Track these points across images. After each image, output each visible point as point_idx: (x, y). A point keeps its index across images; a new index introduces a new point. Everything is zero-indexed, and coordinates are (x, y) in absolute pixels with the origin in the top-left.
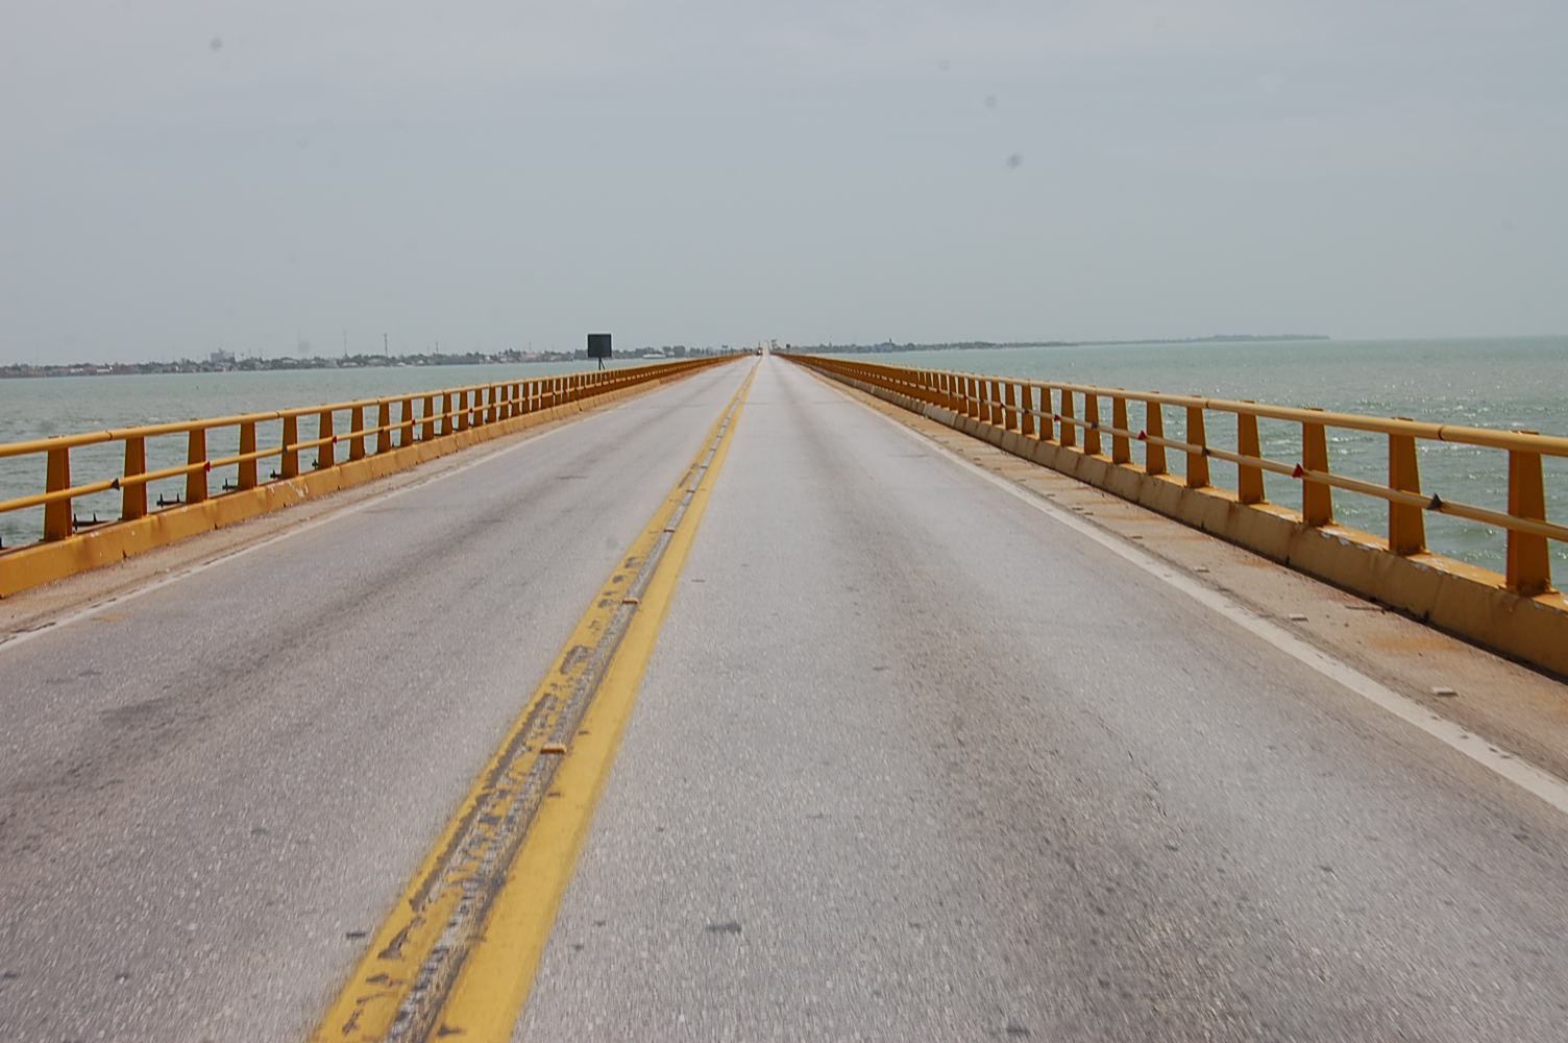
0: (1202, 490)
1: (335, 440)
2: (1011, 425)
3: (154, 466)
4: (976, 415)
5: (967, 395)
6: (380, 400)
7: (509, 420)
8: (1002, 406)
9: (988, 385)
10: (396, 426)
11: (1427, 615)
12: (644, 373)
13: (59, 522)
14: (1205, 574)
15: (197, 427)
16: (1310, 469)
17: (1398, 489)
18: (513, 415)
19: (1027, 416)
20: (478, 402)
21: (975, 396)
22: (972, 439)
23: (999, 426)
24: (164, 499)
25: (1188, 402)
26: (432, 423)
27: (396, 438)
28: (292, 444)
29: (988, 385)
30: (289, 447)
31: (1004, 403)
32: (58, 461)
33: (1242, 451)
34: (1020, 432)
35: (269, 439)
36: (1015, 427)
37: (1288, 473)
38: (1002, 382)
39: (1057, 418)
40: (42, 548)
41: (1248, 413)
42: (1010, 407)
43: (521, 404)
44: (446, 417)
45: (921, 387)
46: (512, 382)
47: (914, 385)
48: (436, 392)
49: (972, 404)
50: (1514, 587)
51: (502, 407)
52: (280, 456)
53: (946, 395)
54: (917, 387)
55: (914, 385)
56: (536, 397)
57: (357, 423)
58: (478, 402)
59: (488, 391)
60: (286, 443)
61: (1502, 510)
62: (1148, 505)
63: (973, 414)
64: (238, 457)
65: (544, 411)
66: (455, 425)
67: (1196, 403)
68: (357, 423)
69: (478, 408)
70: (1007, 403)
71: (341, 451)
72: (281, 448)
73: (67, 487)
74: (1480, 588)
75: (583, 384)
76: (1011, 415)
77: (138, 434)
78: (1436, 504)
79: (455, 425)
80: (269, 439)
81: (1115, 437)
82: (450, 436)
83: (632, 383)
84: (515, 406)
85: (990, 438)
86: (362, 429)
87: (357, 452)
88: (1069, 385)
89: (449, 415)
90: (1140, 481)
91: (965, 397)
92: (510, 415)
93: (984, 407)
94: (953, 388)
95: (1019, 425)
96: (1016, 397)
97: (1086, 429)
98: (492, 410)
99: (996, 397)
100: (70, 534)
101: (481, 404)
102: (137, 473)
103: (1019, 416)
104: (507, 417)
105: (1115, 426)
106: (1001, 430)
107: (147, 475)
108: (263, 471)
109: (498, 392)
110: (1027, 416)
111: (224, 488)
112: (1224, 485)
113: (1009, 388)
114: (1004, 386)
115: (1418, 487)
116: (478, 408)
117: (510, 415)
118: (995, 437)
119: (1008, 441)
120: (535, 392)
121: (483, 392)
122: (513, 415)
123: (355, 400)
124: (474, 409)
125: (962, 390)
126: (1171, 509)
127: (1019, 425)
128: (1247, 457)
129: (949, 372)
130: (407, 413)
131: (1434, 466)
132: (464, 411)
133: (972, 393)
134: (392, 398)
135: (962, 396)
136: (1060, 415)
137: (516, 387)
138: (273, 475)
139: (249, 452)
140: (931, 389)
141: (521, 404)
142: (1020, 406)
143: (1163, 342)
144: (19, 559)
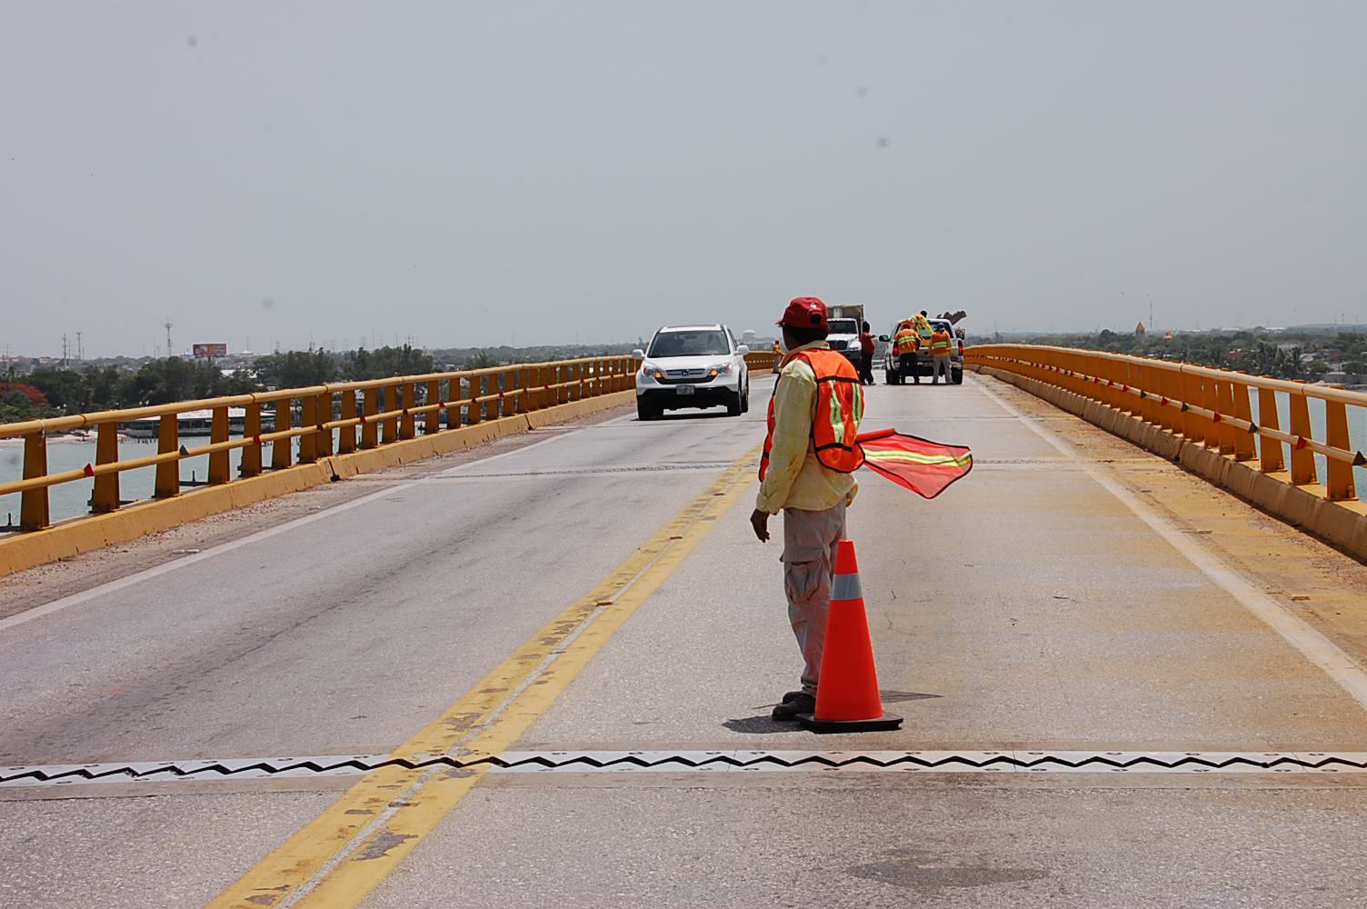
1: (184, 453)
7: (264, 475)
8: (1254, 429)
13: (35, 513)
19: (1301, 446)
22: (1349, 560)
24: (197, 480)
25: (1259, 383)
26: (226, 452)
31: (1257, 421)
42: (1269, 431)
47: (1179, 404)
54: (1143, 395)
70: (1262, 425)
73: (45, 474)
76: (1272, 446)
83: (525, 405)
86: (116, 461)
92: (380, 426)
102: (223, 441)
103: (1286, 450)
105: (1330, 444)
107: (120, 463)
110: (1301, 446)
115: (1349, 446)
122: (342, 451)
124: (95, 468)
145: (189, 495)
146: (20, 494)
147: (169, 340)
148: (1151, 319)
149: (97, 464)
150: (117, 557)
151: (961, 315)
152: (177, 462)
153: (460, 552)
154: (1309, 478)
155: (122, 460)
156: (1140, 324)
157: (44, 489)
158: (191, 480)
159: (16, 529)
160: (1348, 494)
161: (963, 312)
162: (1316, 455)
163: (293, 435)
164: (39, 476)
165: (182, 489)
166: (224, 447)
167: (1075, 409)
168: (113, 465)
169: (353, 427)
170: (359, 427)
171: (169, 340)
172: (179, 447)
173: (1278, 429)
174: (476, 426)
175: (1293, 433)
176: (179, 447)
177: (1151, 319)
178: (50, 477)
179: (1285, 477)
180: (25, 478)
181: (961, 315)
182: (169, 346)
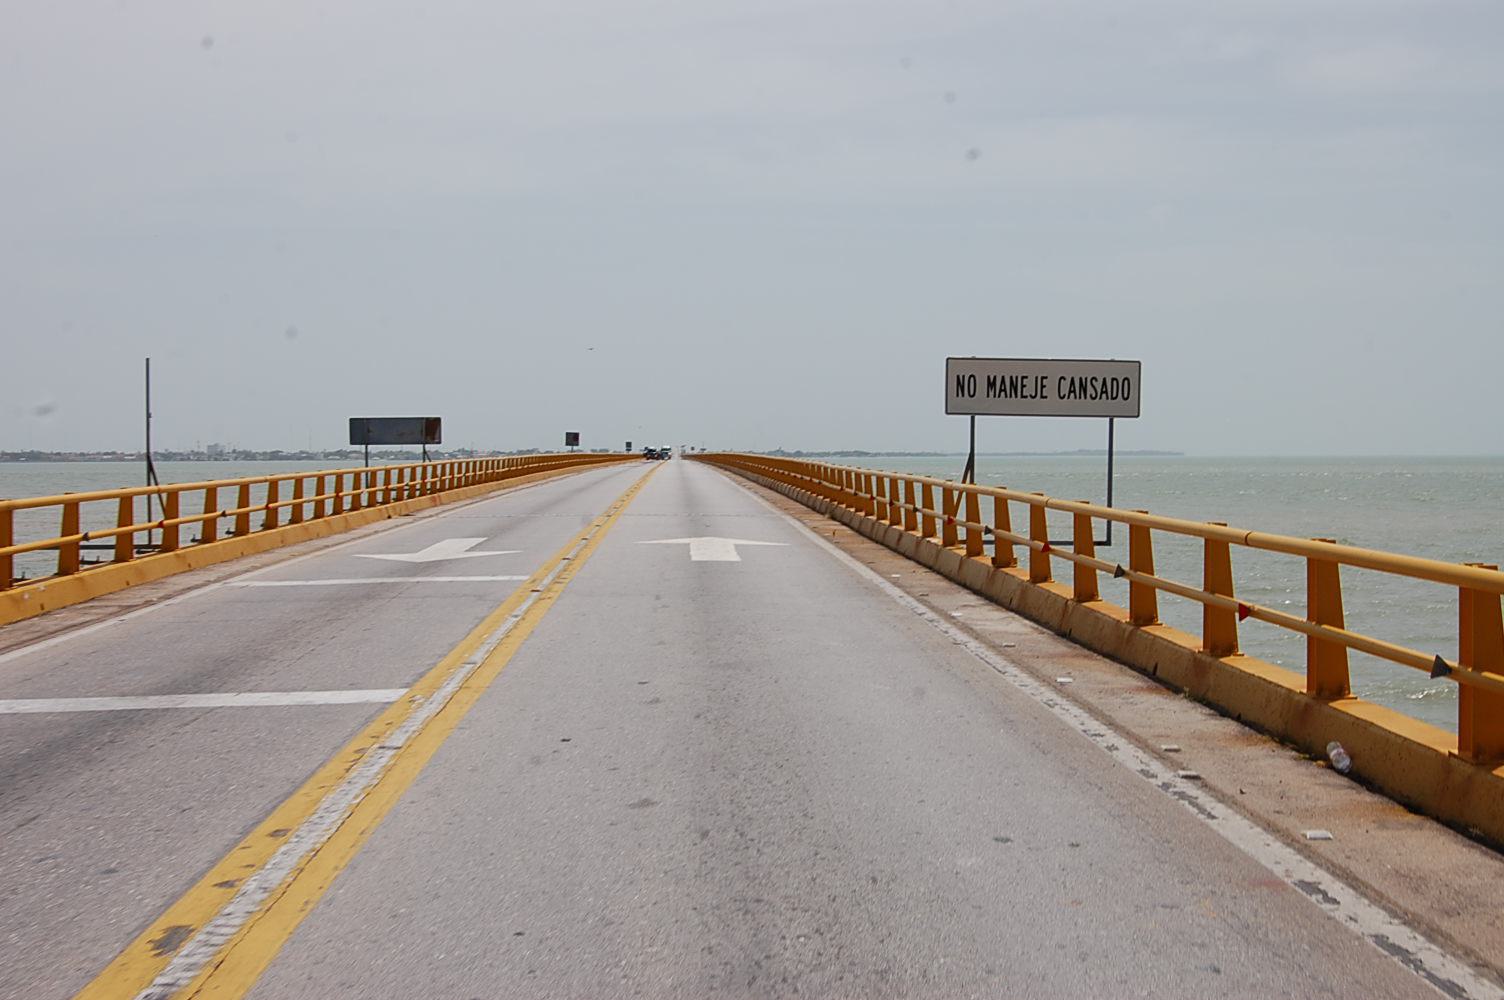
0: (1338, 705)
2: (929, 532)
5: (875, 494)
7: (362, 511)
8: (916, 510)
9: (901, 486)
10: (285, 502)
11: (1240, 715)
14: (925, 598)
15: (173, 489)
16: (1136, 570)
17: (1213, 592)
19: (949, 525)
21: (884, 496)
23: (933, 540)
27: (347, 504)
29: (901, 486)
30: (271, 505)
31: (875, 494)
32: (71, 510)
33: (1209, 586)
35: (258, 497)
36: (914, 528)
37: (1110, 572)
39: (988, 531)
40: (289, 527)
41: (1143, 524)
43: (447, 481)
44: (387, 488)
47: (808, 478)
49: (881, 505)
50: (1469, 754)
52: (264, 512)
53: (885, 504)
54: (811, 480)
55: (808, 478)
57: (298, 492)
59: (383, 472)
60: (269, 502)
61: (1302, 617)
62: (1035, 613)
63: (882, 517)
68: (298, 492)
70: (878, 495)
73: (131, 524)
74: (1262, 682)
76: (929, 521)
78: (1439, 669)
81: (1208, 609)
83: (592, 463)
85: (852, 525)
89: (341, 494)
90: (1024, 589)
91: (872, 498)
92: (447, 487)
94: (859, 488)
95: (920, 526)
96: (900, 492)
97: (944, 522)
98: (338, 500)
99: (910, 498)
100: (78, 570)
103: (939, 525)
104: (414, 497)
106: (899, 531)
108: (185, 537)
112: (1062, 582)
113: (927, 488)
114: (1126, 527)
118: (907, 545)
119: (907, 545)
120: (459, 472)
125: (869, 490)
127: (920, 526)
128: (1081, 555)
129: (855, 469)
131: (1248, 573)
133: (881, 492)
135: (869, 496)
136: (992, 526)
138: (193, 540)
139: (212, 512)
140: (862, 494)
141: (447, 481)
142: (941, 512)
143: (1035, 454)
150: (49, 623)
154: (933, 534)
157: (176, 526)
160: (1046, 578)
162: (958, 527)
163: (181, 523)
170: (438, 483)
173: (1343, 628)
175: (944, 513)
179: (937, 540)
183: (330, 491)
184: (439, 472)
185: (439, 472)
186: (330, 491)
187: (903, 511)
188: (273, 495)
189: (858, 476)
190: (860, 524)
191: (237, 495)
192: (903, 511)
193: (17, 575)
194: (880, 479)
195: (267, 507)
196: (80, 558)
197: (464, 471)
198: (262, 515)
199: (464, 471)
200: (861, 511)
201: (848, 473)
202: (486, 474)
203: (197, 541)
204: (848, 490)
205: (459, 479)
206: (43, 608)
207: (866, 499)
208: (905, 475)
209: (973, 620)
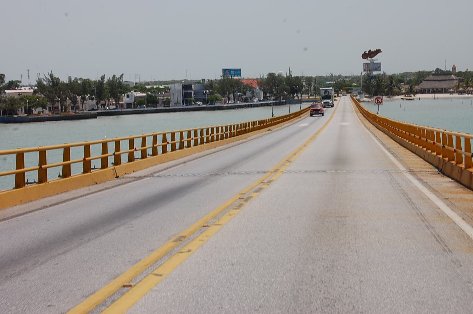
1: (136, 150)
3: (73, 158)
4: (453, 160)
6: (153, 134)
7: (215, 142)
12: (274, 123)
18: (229, 137)
20: (196, 135)
28: (88, 157)
34: (464, 166)
35: (77, 155)
36: (461, 163)
38: (463, 136)
45: (422, 138)
46: (225, 125)
48: (204, 127)
51: (221, 135)
52: (114, 156)
53: (440, 147)
54: (420, 138)
56: (222, 133)
58: (196, 135)
64: (101, 156)
65: (230, 139)
66: (205, 141)
67: (433, 130)
68: (144, 143)
69: (196, 138)
71: (138, 154)
72: (83, 159)
73: (46, 164)
75: (249, 126)
77: (132, 138)
79: (205, 141)
80: (77, 155)
82: (223, 140)
84: (226, 135)
87: (144, 156)
88: (451, 132)
91: (434, 143)
92: (215, 140)
93: (460, 156)
98: (202, 139)
101: (197, 136)
107: (25, 169)
109: (220, 129)
111: (59, 176)
116: (196, 138)
117: (215, 140)
121: (214, 128)
123: (116, 138)
124: (193, 138)
126: (414, 151)
130: (164, 139)
132: (189, 139)
134: (167, 132)
137: (226, 127)
144: (77, 177)
145: (29, 187)
146: (15, 175)
147: (28, 76)
148: (446, 66)
149: (194, 137)
151: (378, 51)
152: (191, 141)
153: (306, 147)
155: (185, 139)
156: (454, 65)
157: (23, 173)
158: (34, 181)
159: (37, 183)
161: (69, 77)
164: (22, 168)
165: (92, 170)
166: (119, 154)
167: (422, 155)
168: (22, 170)
169: (209, 137)
171: (28, 76)
172: (134, 148)
174: (88, 174)
176: (134, 148)
177: (446, 66)
178: (121, 152)
180: (16, 169)
181: (378, 51)
182: (29, 78)
183: (177, 139)
184: (210, 132)
185: (210, 132)
186: (177, 139)
187: (463, 156)
188: (118, 147)
189: (444, 135)
190: (416, 150)
191: (63, 151)
192: (463, 156)
193: (92, 167)
194: (458, 138)
195: (114, 154)
196: (26, 181)
197: (224, 131)
198: (60, 170)
199: (224, 131)
200: (434, 152)
201: (438, 133)
202: (246, 130)
203: (150, 155)
204: (438, 144)
205: (234, 133)
206: (163, 161)
207: (431, 144)
208: (465, 134)
209: (411, 155)
